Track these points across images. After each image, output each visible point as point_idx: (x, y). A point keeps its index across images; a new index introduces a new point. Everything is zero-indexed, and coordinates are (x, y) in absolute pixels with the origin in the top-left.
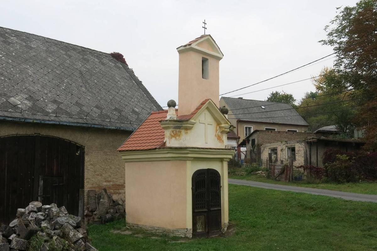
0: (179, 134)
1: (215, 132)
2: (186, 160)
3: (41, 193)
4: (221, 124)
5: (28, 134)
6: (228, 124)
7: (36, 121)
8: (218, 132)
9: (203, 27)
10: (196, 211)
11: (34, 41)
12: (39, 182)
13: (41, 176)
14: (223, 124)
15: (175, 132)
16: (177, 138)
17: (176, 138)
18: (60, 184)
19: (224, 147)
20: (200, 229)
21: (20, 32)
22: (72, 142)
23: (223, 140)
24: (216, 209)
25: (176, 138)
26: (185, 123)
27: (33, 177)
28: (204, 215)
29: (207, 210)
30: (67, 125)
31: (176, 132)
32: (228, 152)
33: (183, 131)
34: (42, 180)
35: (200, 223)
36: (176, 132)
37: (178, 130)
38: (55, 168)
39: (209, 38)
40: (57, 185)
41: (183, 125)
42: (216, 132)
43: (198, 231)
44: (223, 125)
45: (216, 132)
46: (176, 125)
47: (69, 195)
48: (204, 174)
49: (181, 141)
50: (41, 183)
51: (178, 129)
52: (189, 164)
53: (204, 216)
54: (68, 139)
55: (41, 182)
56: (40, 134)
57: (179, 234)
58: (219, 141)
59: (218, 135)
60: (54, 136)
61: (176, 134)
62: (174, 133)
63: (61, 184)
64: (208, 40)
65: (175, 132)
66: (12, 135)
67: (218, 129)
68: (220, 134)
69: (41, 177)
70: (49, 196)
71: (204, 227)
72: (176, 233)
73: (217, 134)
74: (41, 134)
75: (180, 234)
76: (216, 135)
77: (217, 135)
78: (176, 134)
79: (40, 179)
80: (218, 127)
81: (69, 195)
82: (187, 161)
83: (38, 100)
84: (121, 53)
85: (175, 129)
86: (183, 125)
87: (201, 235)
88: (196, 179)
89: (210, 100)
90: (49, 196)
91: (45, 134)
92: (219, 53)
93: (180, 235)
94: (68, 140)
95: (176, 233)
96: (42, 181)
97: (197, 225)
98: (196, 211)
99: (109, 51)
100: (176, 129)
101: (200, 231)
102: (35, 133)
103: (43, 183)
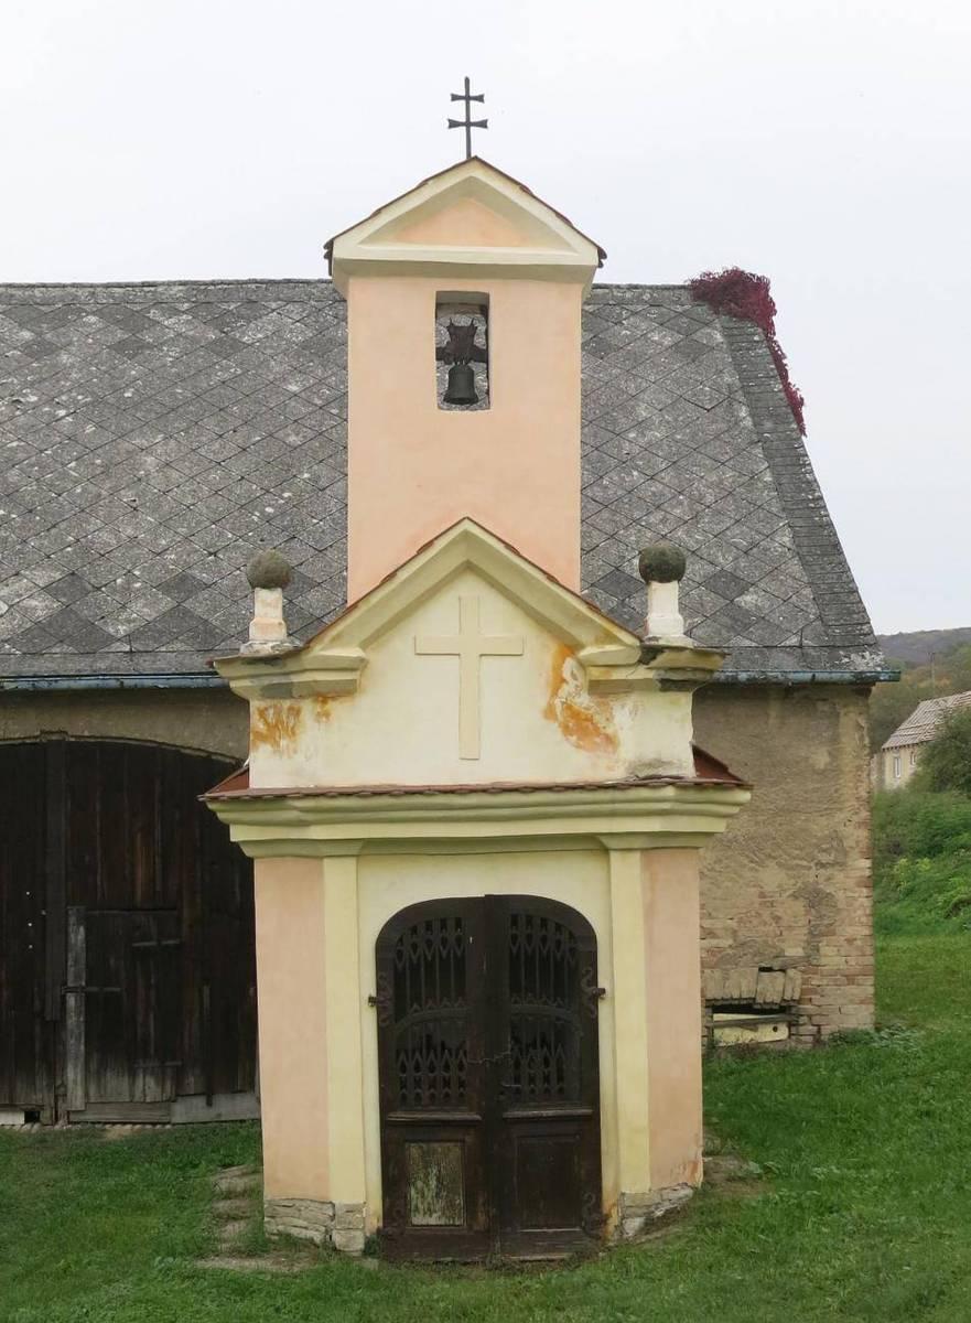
0: (291, 725)
1: (549, 694)
2: (322, 858)
3: (78, 977)
4: (581, 646)
5: (12, 736)
6: (615, 640)
7: (13, 686)
8: (566, 689)
9: (480, 98)
10: (400, 1116)
11: (273, 310)
12: (67, 934)
13: (75, 908)
14: (592, 644)
15: (271, 711)
16: (283, 743)
17: (276, 744)
18: (164, 943)
19: (618, 774)
20: (430, 1212)
21: (230, 283)
22: (214, 757)
23: (609, 731)
24: (545, 1113)
25: (276, 744)
26: (292, 665)
27: (44, 913)
28: (463, 1141)
29: (478, 1117)
30: (156, 689)
31: (278, 713)
32: (613, 802)
33: (308, 708)
34: (79, 924)
35: (433, 1183)
36: (278, 713)
37: (286, 704)
38: (140, 873)
39: (471, 180)
40: (153, 943)
41: (295, 679)
42: (555, 693)
43: (418, 1219)
44: (589, 651)
45: (555, 693)
46: (266, 681)
47: (206, 990)
48: (458, 923)
49: (300, 758)
50: (78, 936)
51: (285, 698)
52: (338, 876)
53: (462, 1149)
54: (196, 747)
55: (77, 933)
56: (66, 733)
57: (301, 1222)
58: (574, 738)
59: (568, 707)
60: (104, 733)
61: (276, 725)
62: (266, 723)
63: (171, 942)
64: (471, 186)
65: (271, 711)
66: (102, 737)
67: (566, 675)
68: (584, 701)
69: (72, 911)
70: (118, 989)
71: (460, 1201)
72: (286, 1220)
73: (557, 702)
74: (70, 733)
75: (305, 1224)
76: (549, 713)
77: (559, 709)
78: (276, 725)
79: (72, 920)
80: (569, 664)
81: (206, 990)
82: (326, 860)
83: (99, 589)
84: (748, 268)
85: (269, 702)
86: (295, 679)
87: (439, 1248)
88: (400, 954)
89: (467, 525)
90: (118, 989)
91: (86, 734)
92: (568, 246)
93: (306, 1228)
94: (199, 750)
95: (286, 1220)
96: (82, 929)
97: (413, 1192)
98: (400, 1116)
99: (682, 273)
100: (275, 702)
101: (433, 1220)
102: (42, 732)
103: (87, 936)
